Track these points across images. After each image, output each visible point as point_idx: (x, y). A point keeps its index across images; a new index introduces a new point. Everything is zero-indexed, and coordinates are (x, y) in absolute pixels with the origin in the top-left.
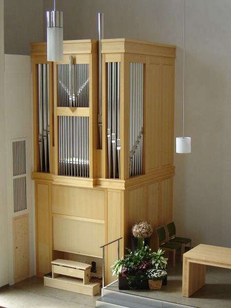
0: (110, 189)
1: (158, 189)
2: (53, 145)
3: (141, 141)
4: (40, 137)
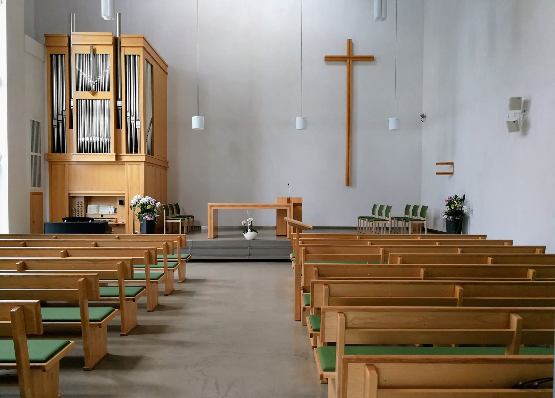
0: (95, 218)
1: (147, 135)
2: (71, 127)
3: (151, 128)
4: (55, 123)
